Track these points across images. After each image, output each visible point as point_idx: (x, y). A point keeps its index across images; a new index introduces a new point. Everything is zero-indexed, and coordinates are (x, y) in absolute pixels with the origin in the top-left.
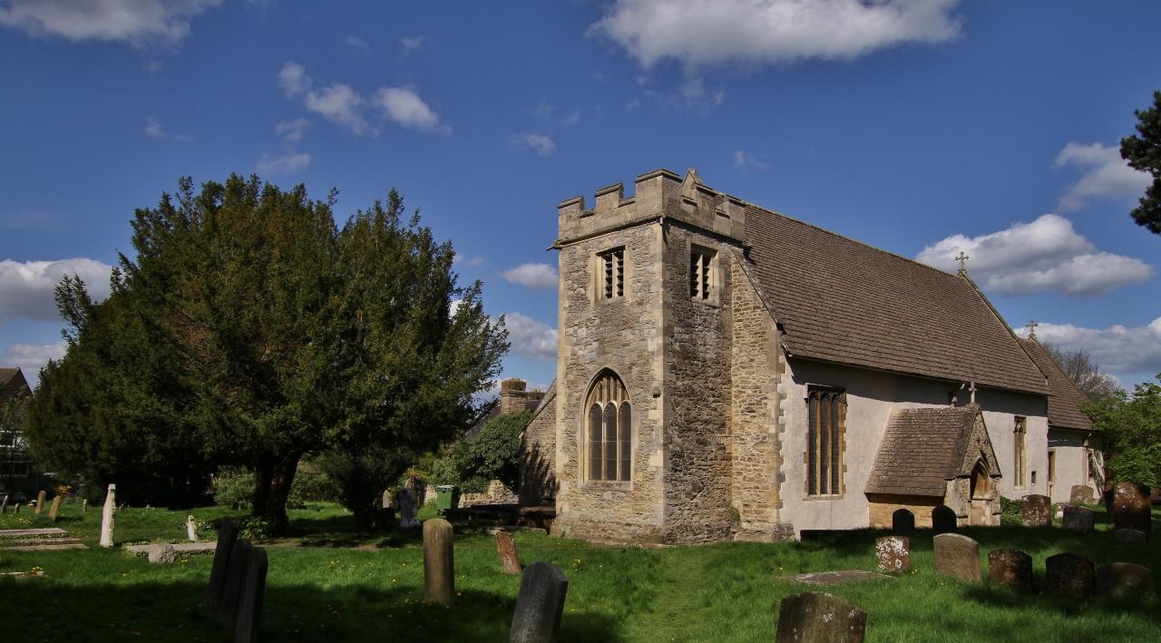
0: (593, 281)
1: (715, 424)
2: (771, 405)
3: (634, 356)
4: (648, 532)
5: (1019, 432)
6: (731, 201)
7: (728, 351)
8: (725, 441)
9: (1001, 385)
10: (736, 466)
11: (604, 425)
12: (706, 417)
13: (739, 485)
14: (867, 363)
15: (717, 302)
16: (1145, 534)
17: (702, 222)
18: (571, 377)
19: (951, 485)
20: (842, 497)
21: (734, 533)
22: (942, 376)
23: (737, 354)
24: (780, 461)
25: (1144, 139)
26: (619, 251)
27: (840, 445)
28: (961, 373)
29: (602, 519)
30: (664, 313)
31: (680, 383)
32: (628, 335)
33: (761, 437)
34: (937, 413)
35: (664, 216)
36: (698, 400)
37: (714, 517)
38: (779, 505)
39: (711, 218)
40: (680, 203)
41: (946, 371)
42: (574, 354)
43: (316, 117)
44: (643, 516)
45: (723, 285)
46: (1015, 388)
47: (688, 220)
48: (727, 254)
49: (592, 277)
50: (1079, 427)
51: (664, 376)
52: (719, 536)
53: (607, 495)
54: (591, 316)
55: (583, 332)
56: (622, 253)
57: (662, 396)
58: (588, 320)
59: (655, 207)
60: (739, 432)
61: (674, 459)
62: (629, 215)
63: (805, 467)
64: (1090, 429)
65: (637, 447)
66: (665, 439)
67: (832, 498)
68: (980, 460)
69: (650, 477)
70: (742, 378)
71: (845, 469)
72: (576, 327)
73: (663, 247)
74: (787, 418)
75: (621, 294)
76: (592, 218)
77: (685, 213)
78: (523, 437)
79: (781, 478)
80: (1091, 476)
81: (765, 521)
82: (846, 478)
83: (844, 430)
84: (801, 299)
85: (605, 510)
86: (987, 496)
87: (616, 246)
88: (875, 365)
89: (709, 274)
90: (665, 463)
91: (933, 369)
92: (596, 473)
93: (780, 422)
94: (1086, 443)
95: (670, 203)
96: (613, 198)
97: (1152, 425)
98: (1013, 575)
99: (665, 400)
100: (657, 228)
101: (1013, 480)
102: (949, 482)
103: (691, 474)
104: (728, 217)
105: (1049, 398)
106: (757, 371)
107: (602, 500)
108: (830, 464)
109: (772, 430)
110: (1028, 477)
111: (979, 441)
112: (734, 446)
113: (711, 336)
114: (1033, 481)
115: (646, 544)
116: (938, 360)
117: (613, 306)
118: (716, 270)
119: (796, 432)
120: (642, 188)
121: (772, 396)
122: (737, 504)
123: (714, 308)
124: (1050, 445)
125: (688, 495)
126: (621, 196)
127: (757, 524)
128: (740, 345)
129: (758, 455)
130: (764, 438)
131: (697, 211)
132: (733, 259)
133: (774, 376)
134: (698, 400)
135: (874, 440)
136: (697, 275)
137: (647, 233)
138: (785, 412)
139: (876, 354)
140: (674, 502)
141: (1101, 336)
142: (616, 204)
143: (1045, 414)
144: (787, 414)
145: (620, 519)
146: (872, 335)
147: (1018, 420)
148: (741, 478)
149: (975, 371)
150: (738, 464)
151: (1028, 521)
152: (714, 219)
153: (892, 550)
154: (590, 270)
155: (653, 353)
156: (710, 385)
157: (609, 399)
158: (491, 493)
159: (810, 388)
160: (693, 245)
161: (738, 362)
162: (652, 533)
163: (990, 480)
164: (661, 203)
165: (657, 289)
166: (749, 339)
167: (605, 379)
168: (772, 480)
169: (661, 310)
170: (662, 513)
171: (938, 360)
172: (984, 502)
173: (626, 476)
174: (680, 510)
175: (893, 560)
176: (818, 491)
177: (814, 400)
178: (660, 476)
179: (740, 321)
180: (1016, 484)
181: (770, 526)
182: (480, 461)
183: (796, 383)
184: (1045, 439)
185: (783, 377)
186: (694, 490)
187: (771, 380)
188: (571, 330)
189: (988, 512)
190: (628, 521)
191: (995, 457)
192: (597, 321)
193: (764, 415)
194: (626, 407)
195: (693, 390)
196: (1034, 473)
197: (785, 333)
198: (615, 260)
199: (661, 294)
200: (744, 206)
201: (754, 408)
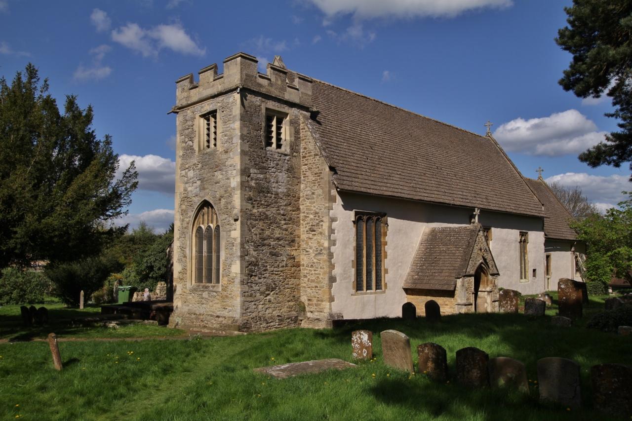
0: (197, 136)
1: (286, 241)
2: (325, 226)
3: (222, 191)
4: (230, 322)
5: (523, 242)
6: (299, 78)
7: (297, 187)
8: (294, 253)
9: (507, 210)
10: (304, 271)
11: (205, 243)
12: (277, 235)
13: (305, 285)
14: (402, 195)
15: (288, 151)
16: (570, 320)
17: (275, 93)
18: (184, 207)
19: (459, 282)
20: (384, 292)
21: (301, 320)
22: (462, 204)
23: (304, 189)
24: (332, 266)
25: (573, 29)
26: (213, 113)
27: (383, 254)
28: (478, 202)
29: (202, 312)
30: (241, 159)
31: (255, 211)
32: (219, 175)
33: (319, 250)
34: (453, 230)
35: (241, 87)
36: (271, 223)
37: (285, 309)
38: (332, 299)
39: (283, 90)
40: (256, 77)
41: (466, 201)
42: (185, 190)
43: (118, 46)
44: (227, 310)
45: (293, 139)
46: (518, 212)
47: (263, 90)
48: (296, 116)
49: (197, 133)
50: (567, 238)
51: (241, 206)
52: (289, 324)
53: (205, 295)
54: (196, 162)
55: (191, 174)
56: (216, 115)
57: (239, 221)
58: (194, 164)
59: (236, 81)
60: (305, 246)
61: (250, 267)
62: (220, 87)
63: (353, 271)
64: (574, 239)
65: (224, 259)
66: (241, 252)
67: (375, 293)
68: (482, 263)
69: (232, 281)
70: (307, 206)
71: (386, 271)
72: (187, 170)
73: (241, 109)
74: (337, 235)
75: (215, 145)
76: (197, 89)
77: (260, 85)
78: (169, 252)
79: (332, 279)
80: (577, 271)
81: (321, 312)
82: (387, 278)
83: (386, 244)
84: (355, 149)
85: (204, 306)
86: (488, 289)
87: (212, 110)
88: (409, 197)
89: (282, 130)
90: (241, 271)
91: (456, 199)
92: (199, 279)
93: (332, 238)
94: (573, 249)
95: (247, 77)
96: (210, 75)
97: (614, 237)
98: (433, 364)
99: (242, 223)
100: (237, 96)
101: (519, 275)
102: (458, 280)
103: (265, 278)
104: (297, 89)
105: (545, 219)
106: (316, 201)
107: (202, 298)
108: (374, 268)
109: (326, 244)
110: (530, 273)
111: (481, 250)
112: (302, 257)
113: (283, 176)
114: (534, 275)
115: (228, 331)
116: (461, 193)
117: (209, 154)
118: (288, 128)
119: (345, 246)
120: (228, 67)
121: (326, 219)
122: (304, 299)
123: (286, 155)
124: (546, 251)
125: (262, 293)
126: (216, 73)
127: (316, 314)
128: (305, 182)
129: (317, 263)
130: (321, 250)
131: (271, 84)
132: (302, 120)
133: (327, 205)
134: (271, 223)
135: (410, 250)
136: (272, 131)
137: (231, 100)
138: (336, 231)
139: (411, 189)
140: (249, 299)
141: (605, 181)
142: (212, 79)
143: (542, 230)
144: (338, 233)
145: (213, 312)
146: (410, 175)
147: (522, 234)
148: (306, 279)
149: (489, 201)
150: (304, 270)
151: (503, 309)
152: (286, 91)
153: (361, 341)
154: (196, 128)
155: (234, 189)
156: (282, 212)
157: (208, 224)
158: (158, 291)
159: (356, 213)
160: (267, 109)
161: (305, 195)
162: (232, 323)
163: (490, 277)
164: (239, 77)
165: (237, 141)
166: (312, 178)
167: (205, 208)
168: (326, 281)
169: (239, 156)
170: (239, 308)
171: (461, 193)
172: (486, 293)
173: (218, 281)
174: (255, 305)
175: (361, 349)
176: (365, 288)
177: (361, 222)
178: (238, 280)
179: (306, 165)
180: (521, 278)
181: (325, 315)
182: (151, 268)
183: (345, 209)
184: (543, 247)
185: (334, 205)
186: (267, 290)
187: (325, 208)
188: (183, 172)
189: (489, 300)
190: (218, 313)
191: (493, 260)
192: (200, 166)
193: (321, 233)
194: (218, 226)
195: (267, 216)
196: (534, 270)
197: (336, 173)
198: (212, 120)
199: (239, 144)
200: (311, 82)
201: (315, 228)
